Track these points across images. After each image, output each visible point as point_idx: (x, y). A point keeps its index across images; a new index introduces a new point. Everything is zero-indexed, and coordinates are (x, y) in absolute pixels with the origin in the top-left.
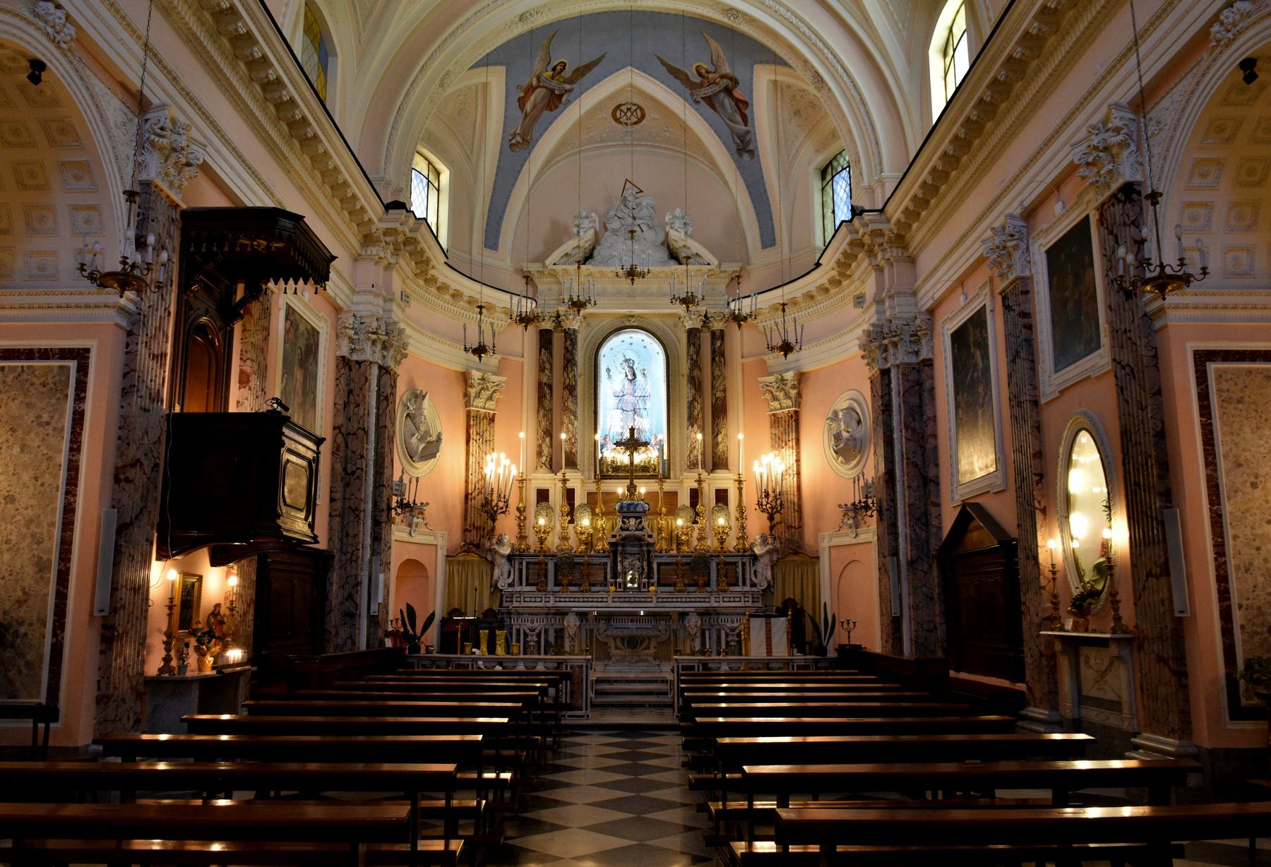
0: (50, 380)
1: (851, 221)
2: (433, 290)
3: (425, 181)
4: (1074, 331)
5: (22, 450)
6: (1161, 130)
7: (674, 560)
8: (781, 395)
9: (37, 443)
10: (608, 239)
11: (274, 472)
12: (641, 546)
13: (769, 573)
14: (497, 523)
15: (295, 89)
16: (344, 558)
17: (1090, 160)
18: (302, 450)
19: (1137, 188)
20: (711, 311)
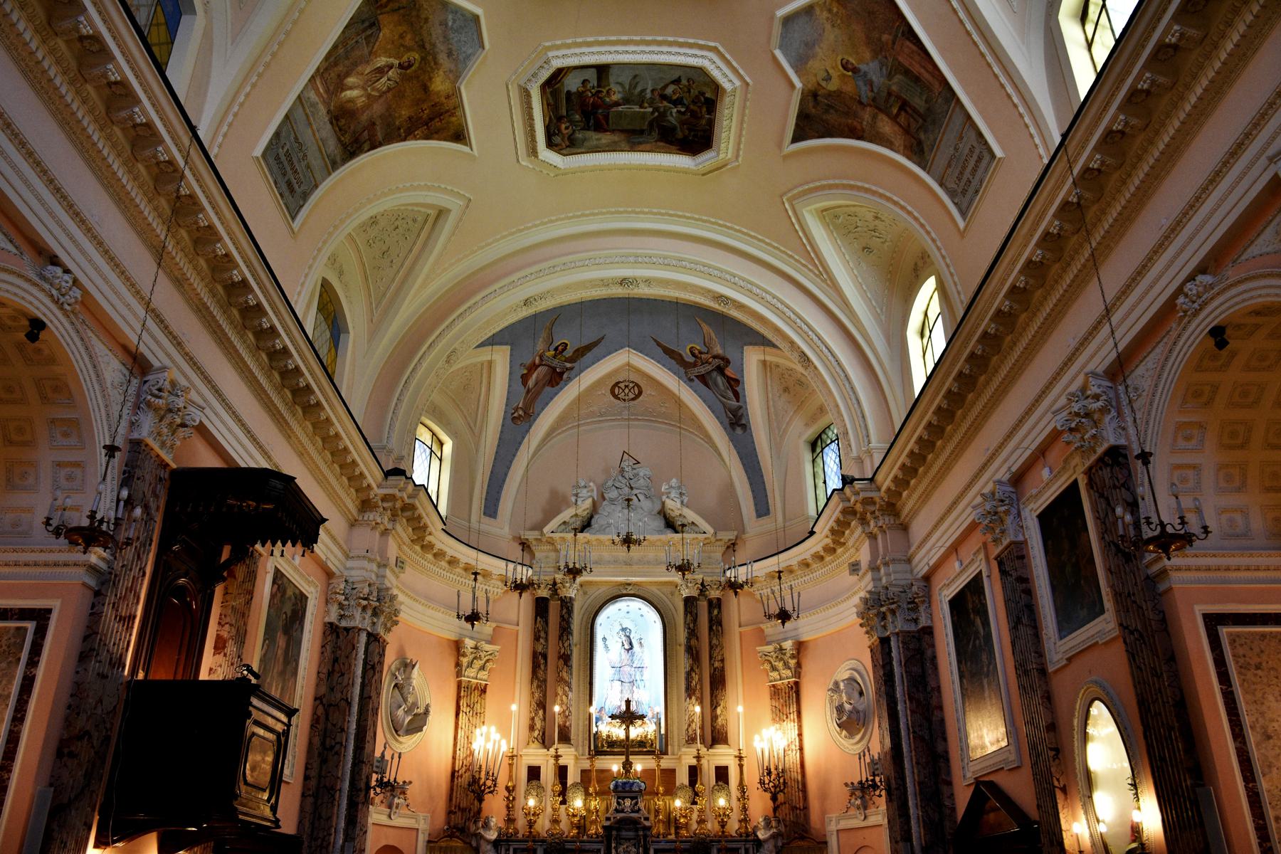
1: (842, 489)
2: (430, 556)
3: (428, 451)
4: (1076, 598)
6: (1139, 396)
7: (672, 846)
8: (780, 665)
10: (605, 508)
11: (237, 746)
12: (637, 830)
14: (484, 805)
15: (300, 358)
17: (1073, 425)
18: (270, 722)
20: (708, 579)
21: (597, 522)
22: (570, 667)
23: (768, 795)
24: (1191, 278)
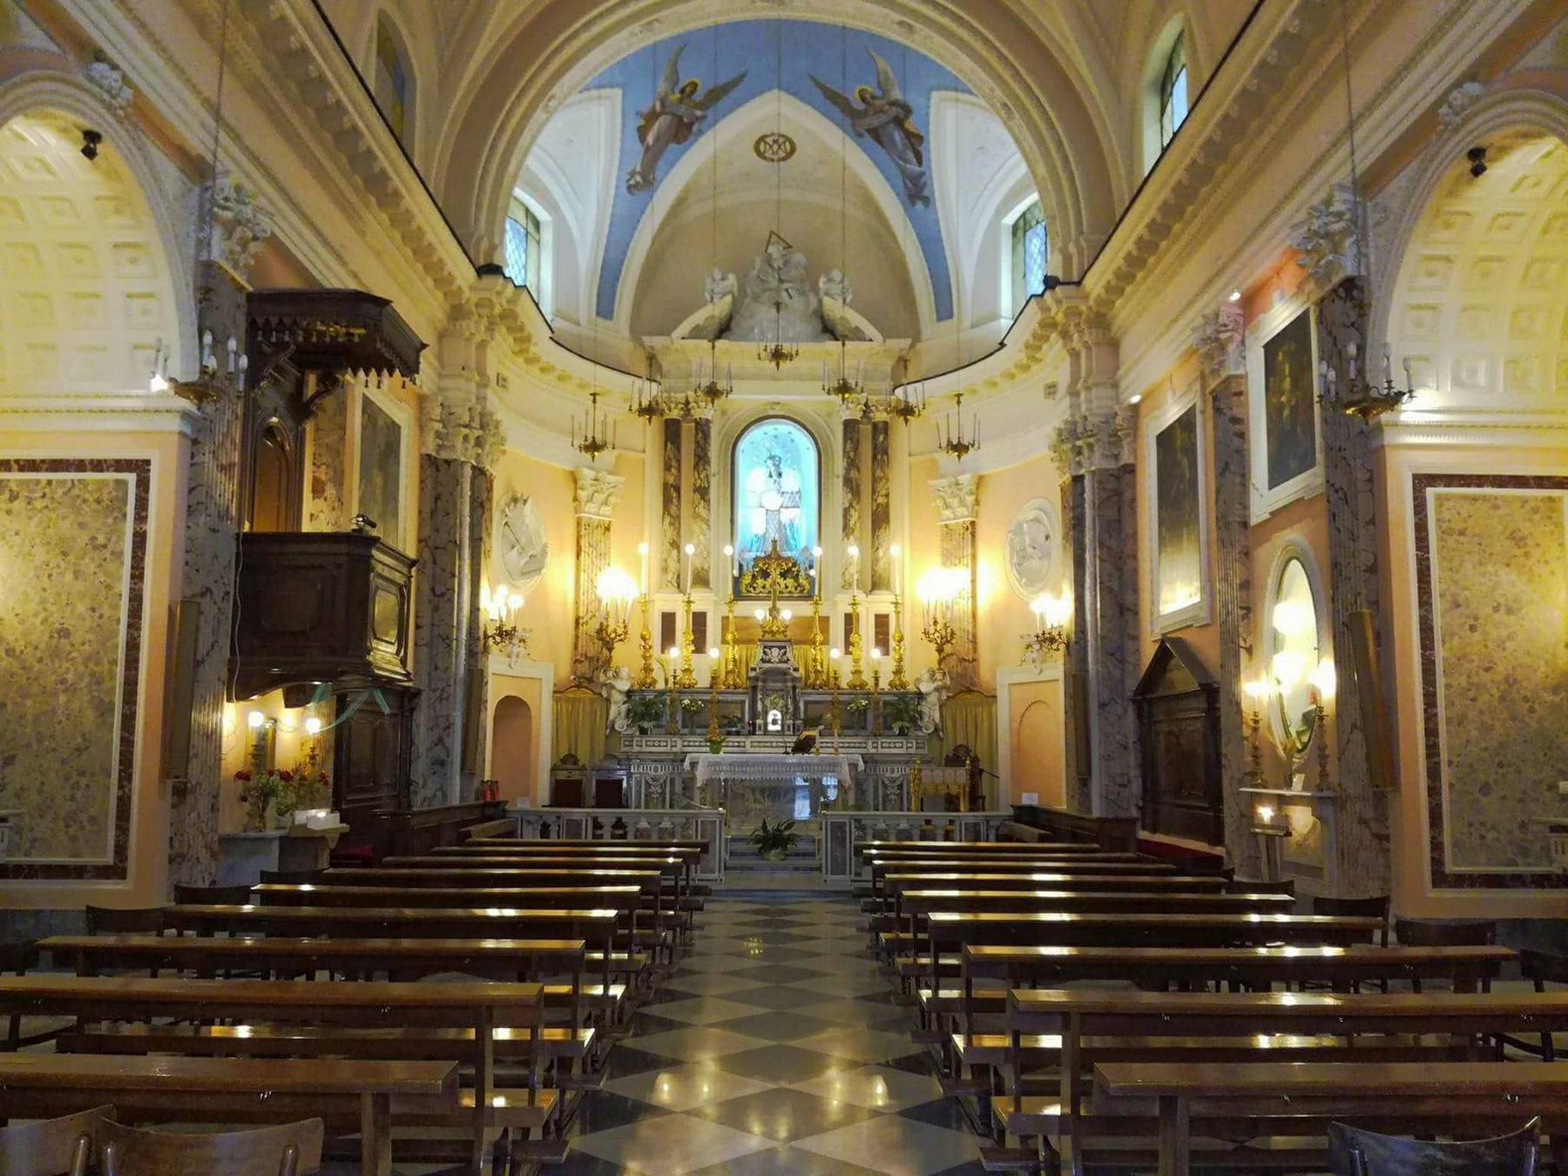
0: (105, 497)
1: (1042, 295)
5: (76, 578)
6: (1387, 218)
8: (955, 502)
9: (92, 568)
19: (1360, 283)
20: (873, 399)
21: (740, 324)
22: (707, 502)
24: (1458, 84)
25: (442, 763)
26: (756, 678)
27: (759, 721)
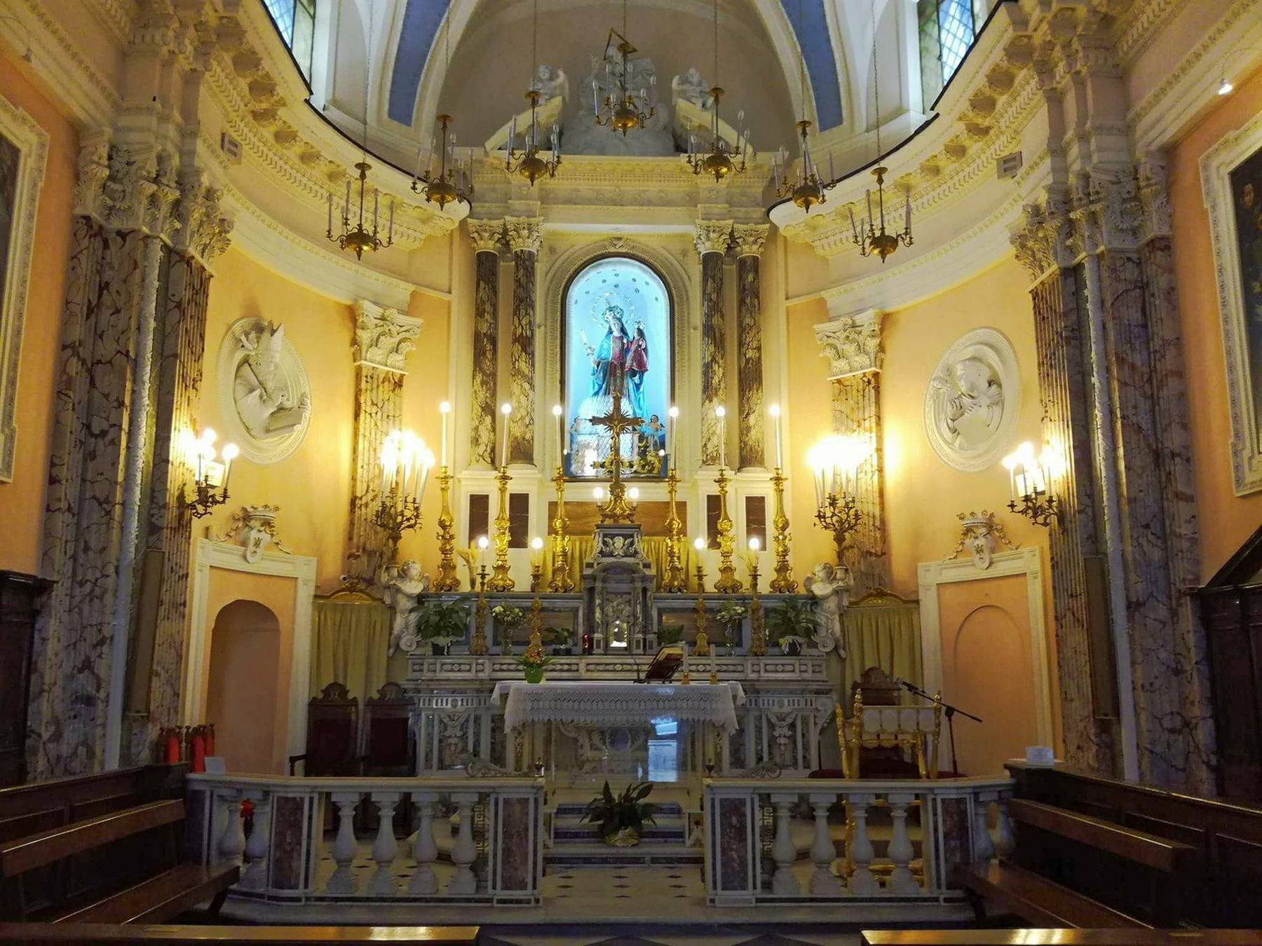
8: (850, 349)
12: (633, 581)
13: (837, 627)
14: (400, 543)
16: (77, 591)
22: (531, 355)
23: (830, 534)
25: (89, 701)
26: (593, 578)
27: (597, 636)
